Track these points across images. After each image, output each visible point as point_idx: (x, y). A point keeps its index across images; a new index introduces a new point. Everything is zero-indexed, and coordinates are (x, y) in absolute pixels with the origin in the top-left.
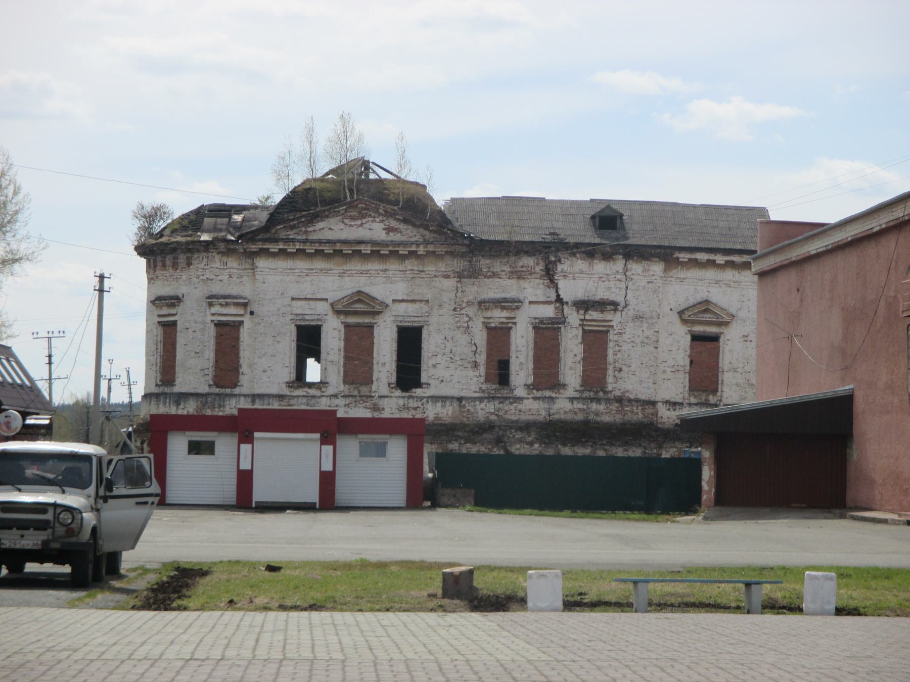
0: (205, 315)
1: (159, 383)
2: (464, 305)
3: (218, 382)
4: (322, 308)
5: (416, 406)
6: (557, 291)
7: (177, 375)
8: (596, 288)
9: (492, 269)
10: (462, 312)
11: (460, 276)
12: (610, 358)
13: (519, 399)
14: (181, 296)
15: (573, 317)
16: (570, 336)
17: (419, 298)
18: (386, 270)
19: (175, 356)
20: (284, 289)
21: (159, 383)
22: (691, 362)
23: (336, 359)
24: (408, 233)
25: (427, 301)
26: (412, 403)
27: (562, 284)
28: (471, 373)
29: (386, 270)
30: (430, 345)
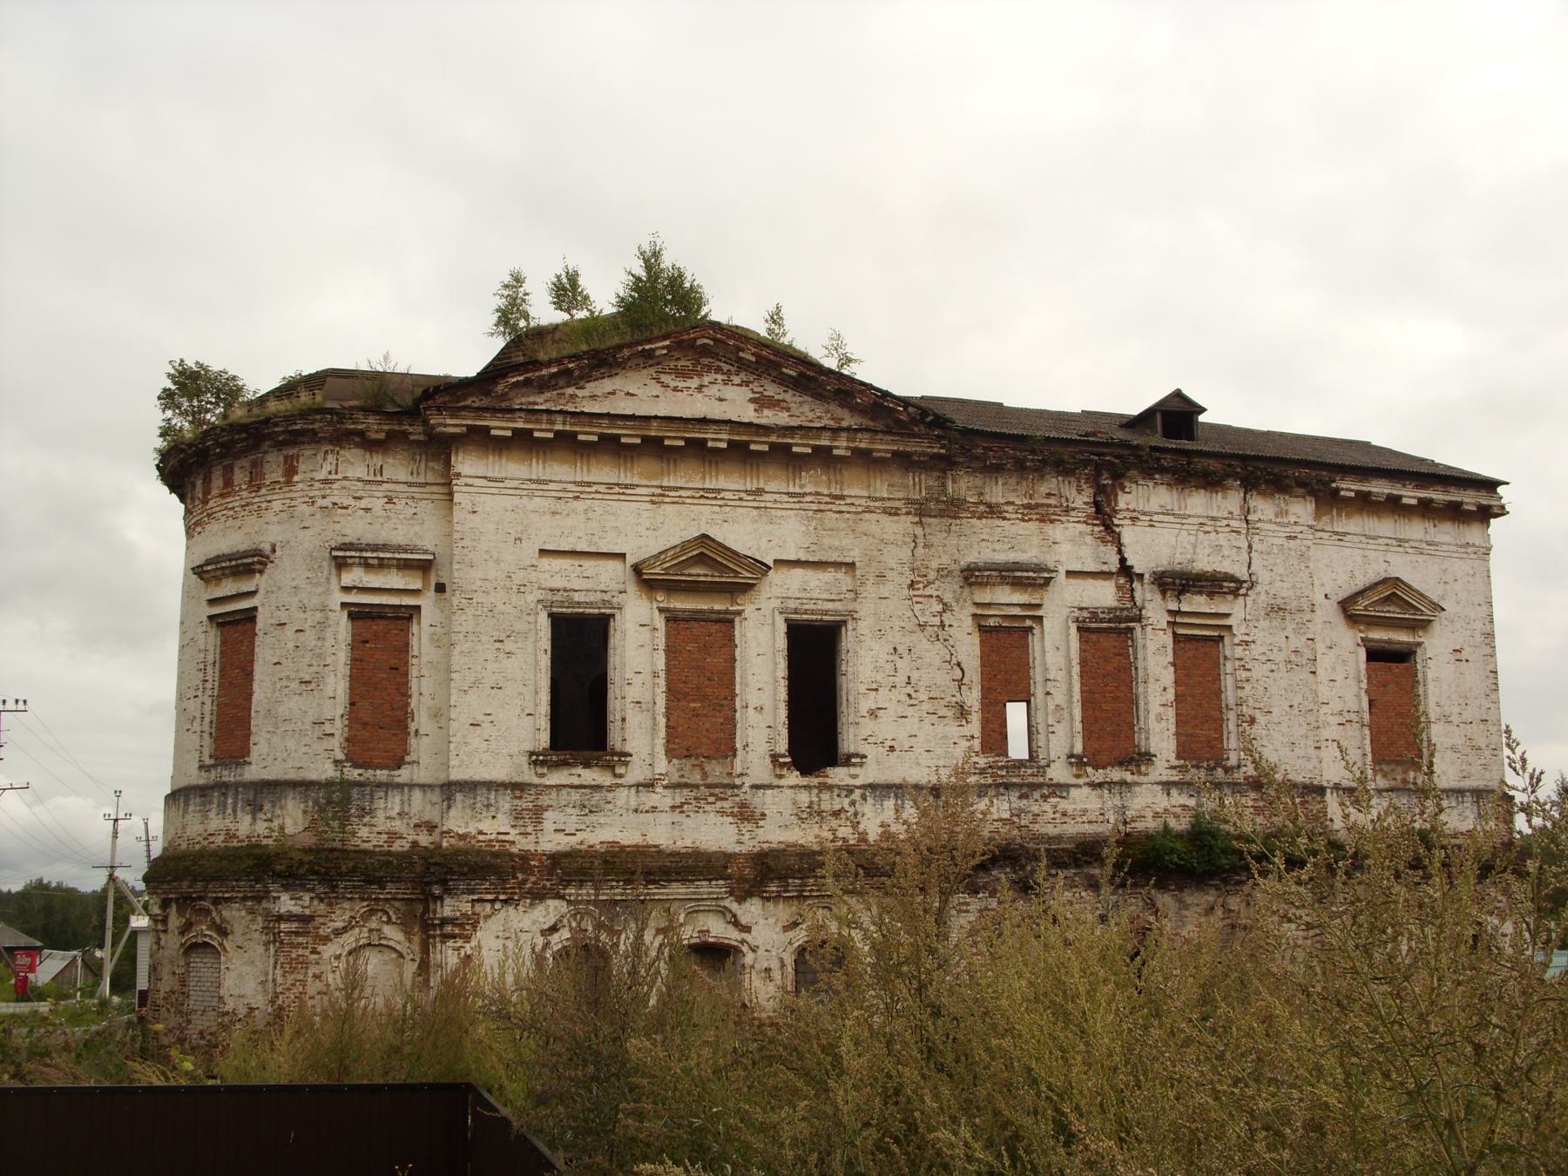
0: (327, 592)
1: (208, 761)
2: (932, 575)
3: (357, 752)
4: (610, 575)
5: (837, 807)
6: (1120, 552)
7: (253, 739)
8: (1195, 547)
9: (987, 498)
10: (928, 591)
11: (921, 511)
12: (1230, 696)
13: (1060, 789)
14: (267, 548)
15: (1156, 609)
16: (1151, 647)
17: (834, 557)
18: (760, 492)
19: (250, 694)
20: (524, 537)
21: (208, 761)
22: (1371, 703)
23: (648, 697)
24: (800, 411)
25: (852, 565)
26: (829, 802)
27: (1128, 534)
28: (954, 730)
29: (760, 492)
30: (864, 665)
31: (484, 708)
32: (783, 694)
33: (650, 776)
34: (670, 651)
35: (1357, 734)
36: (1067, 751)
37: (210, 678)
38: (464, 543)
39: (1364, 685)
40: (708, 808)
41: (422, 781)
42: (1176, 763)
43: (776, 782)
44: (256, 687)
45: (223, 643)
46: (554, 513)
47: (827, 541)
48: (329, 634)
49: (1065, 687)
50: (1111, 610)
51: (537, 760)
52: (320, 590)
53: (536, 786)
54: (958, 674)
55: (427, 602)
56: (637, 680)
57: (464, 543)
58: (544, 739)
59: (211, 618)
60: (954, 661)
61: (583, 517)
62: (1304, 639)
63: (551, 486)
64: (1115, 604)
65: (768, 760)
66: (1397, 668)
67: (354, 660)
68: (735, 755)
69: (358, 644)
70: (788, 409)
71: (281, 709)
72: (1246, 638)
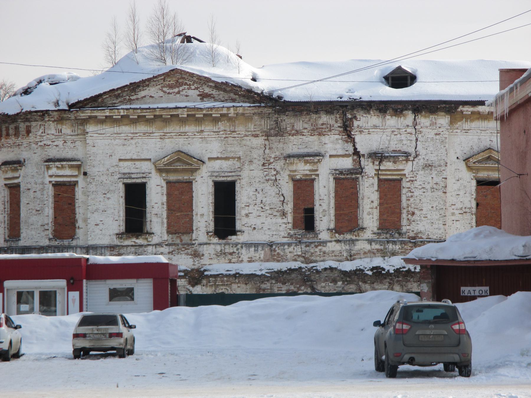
0: (44, 177)
1: (7, 238)
5: (232, 251)
6: (354, 146)
7: (21, 231)
8: (389, 141)
10: (270, 167)
12: (404, 203)
13: (324, 243)
14: (22, 160)
15: (370, 167)
18: (202, 131)
21: (7, 238)
22: (478, 205)
25: (239, 158)
26: (228, 249)
27: (358, 138)
28: (280, 220)
29: (202, 131)
30: (243, 196)
31: (101, 219)
32: (211, 208)
33: (161, 241)
34: (169, 195)
35: (469, 217)
36: (327, 227)
40: (182, 252)
42: (377, 231)
43: (209, 242)
44: (21, 212)
45: (11, 194)
46: (124, 145)
48: (45, 193)
49: (327, 202)
50: (349, 170)
51: (119, 235)
52: (41, 176)
53: (119, 246)
54: (282, 199)
55: (80, 179)
56: (156, 206)
58: (123, 228)
59: (5, 185)
60: (281, 193)
61: (134, 146)
63: (122, 135)
64: (352, 167)
66: (492, 188)
67: (55, 201)
68: (193, 232)
70: (214, 98)
72: (412, 179)
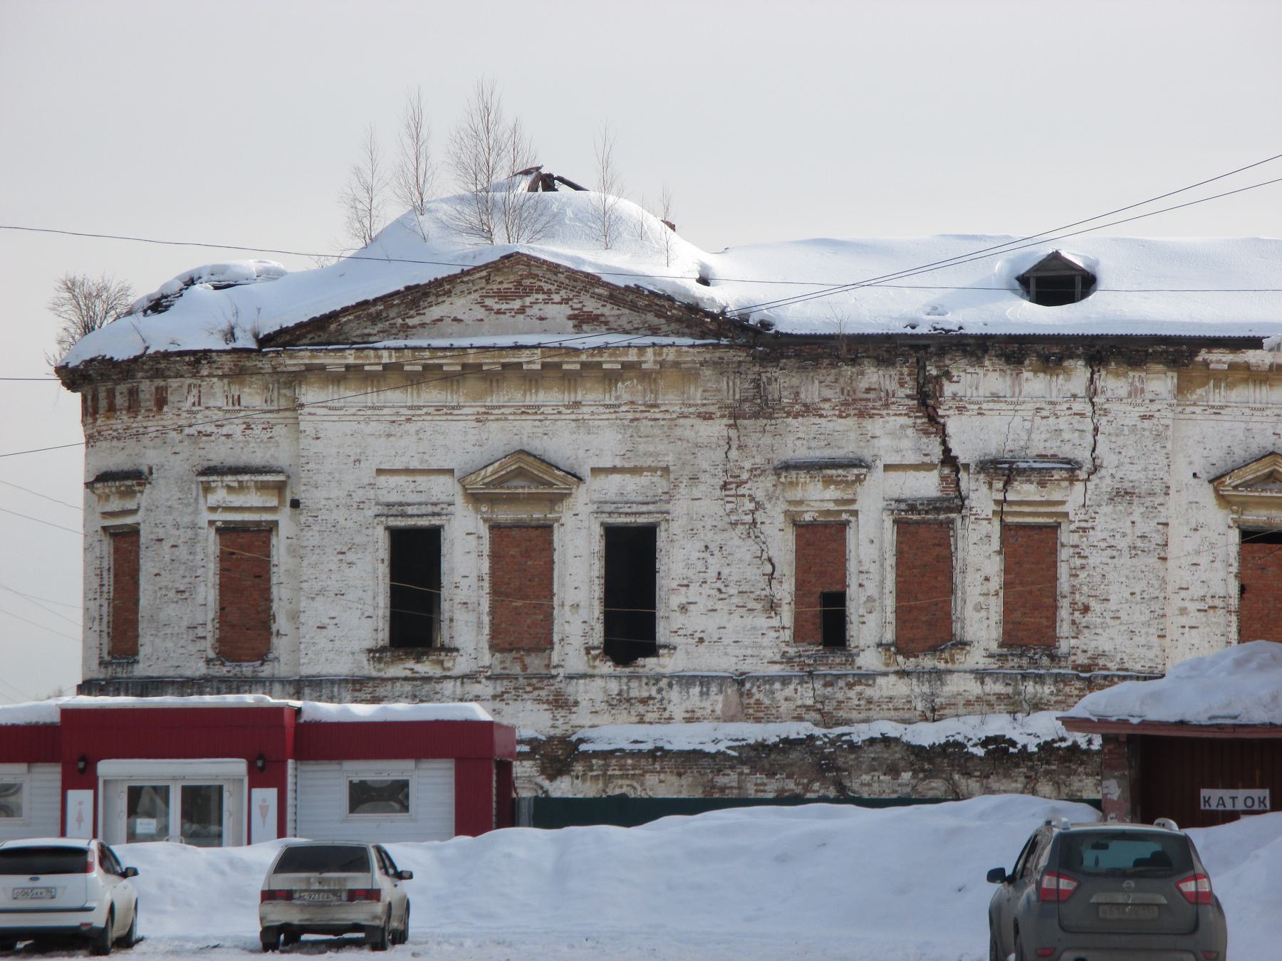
0: (196, 512)
5: (645, 694)
6: (944, 443)
7: (141, 641)
8: (1030, 432)
10: (741, 491)
12: (1064, 583)
13: (868, 678)
14: (146, 470)
15: (981, 496)
16: (974, 537)
18: (577, 404)
20: (366, 455)
21: (107, 658)
22: (1243, 589)
25: (666, 470)
26: (638, 690)
27: (954, 425)
28: (762, 622)
30: (675, 563)
31: (332, 613)
32: (598, 591)
33: (475, 669)
34: (495, 557)
36: (877, 640)
37: (105, 582)
38: (307, 467)
39: (1234, 569)
40: (525, 696)
41: (283, 674)
43: (590, 671)
44: (141, 595)
45: (116, 550)
46: (389, 435)
47: (642, 448)
48: (199, 549)
49: (877, 578)
50: (931, 501)
51: (376, 654)
54: (769, 569)
55: (284, 518)
56: (464, 583)
57: (307, 467)
58: (383, 637)
59: (104, 528)
62: (1153, 523)
63: (386, 411)
64: (939, 494)
65: (583, 652)
68: (552, 648)
69: (226, 559)
70: (606, 323)
71: (161, 615)
72: (1084, 525)
